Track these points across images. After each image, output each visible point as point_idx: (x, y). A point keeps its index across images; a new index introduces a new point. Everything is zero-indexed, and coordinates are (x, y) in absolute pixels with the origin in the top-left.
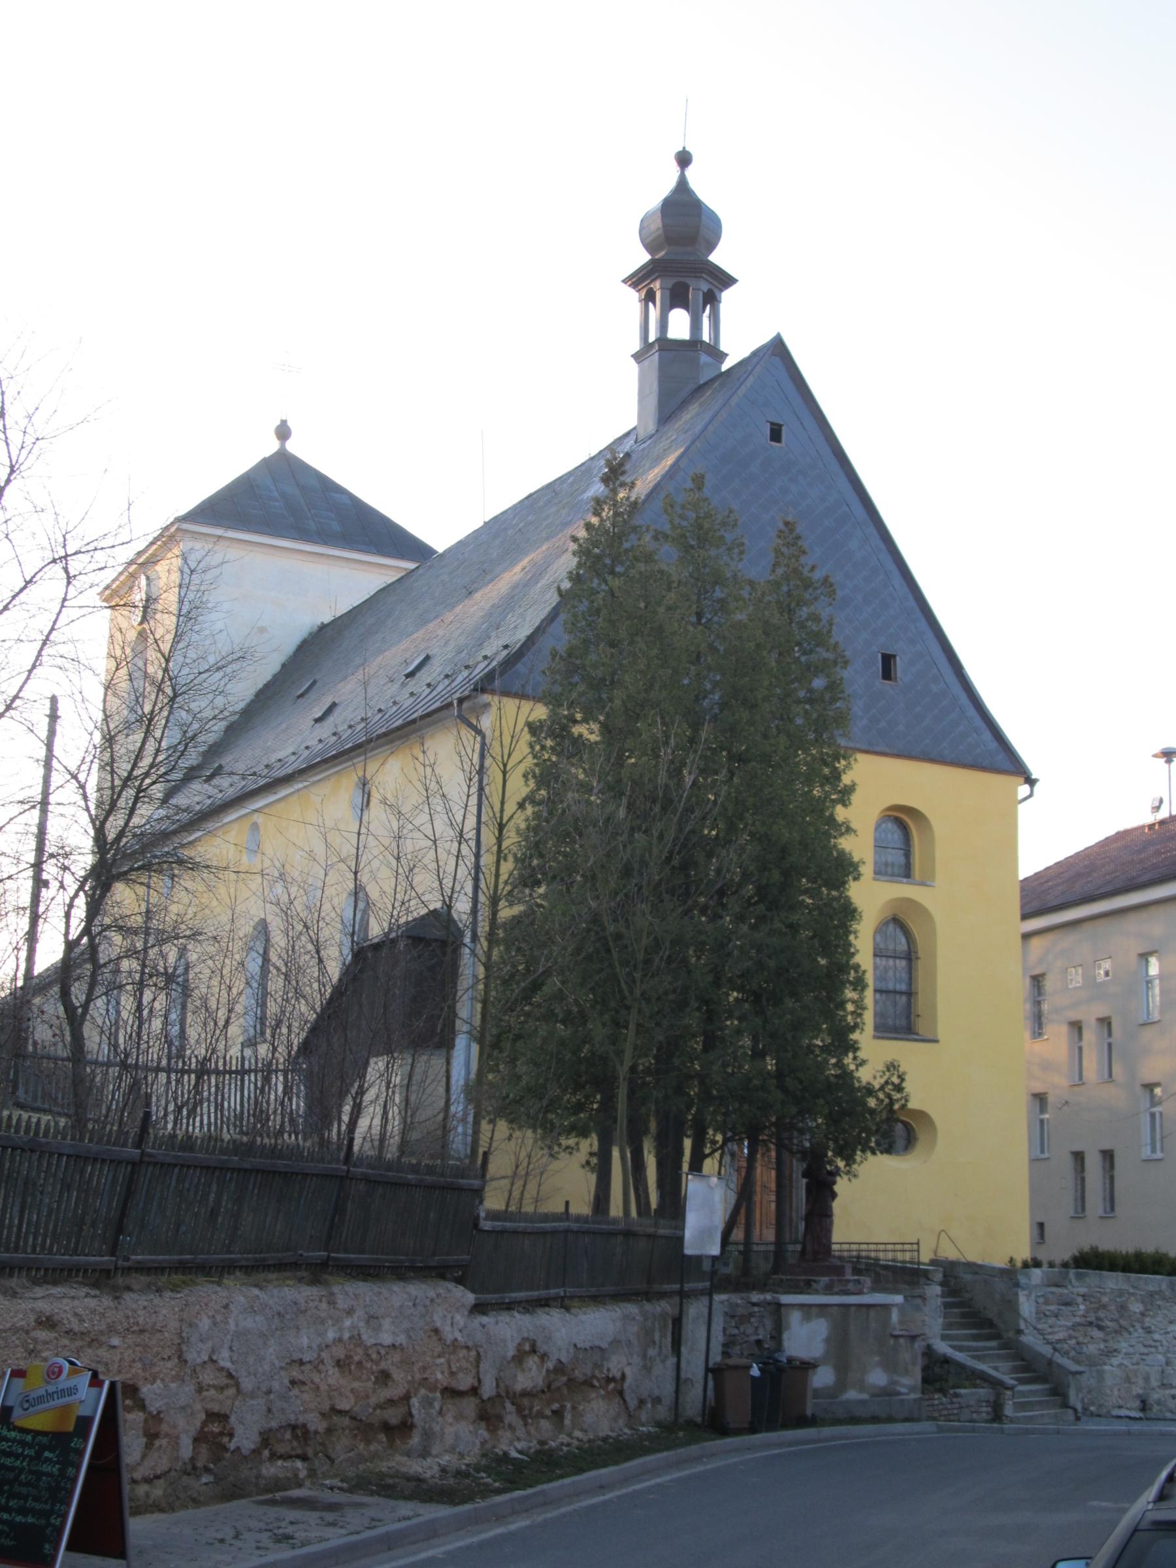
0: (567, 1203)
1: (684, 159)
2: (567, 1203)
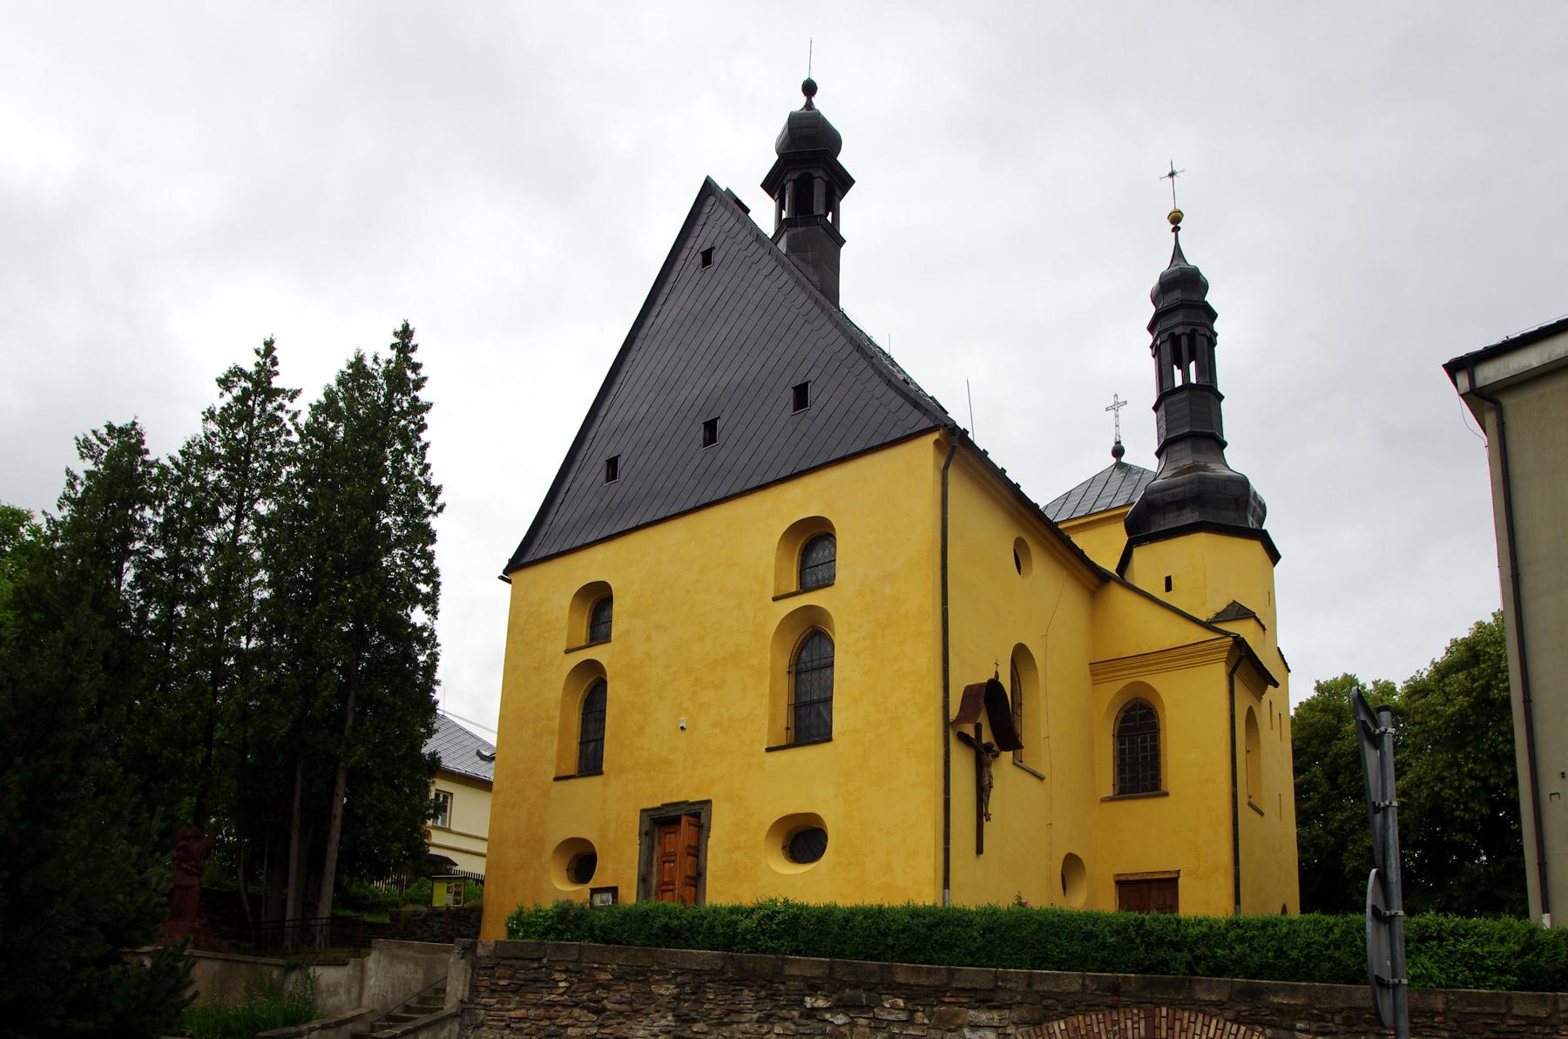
0: (1183, 317)
1: (809, 88)
2: (1183, 317)
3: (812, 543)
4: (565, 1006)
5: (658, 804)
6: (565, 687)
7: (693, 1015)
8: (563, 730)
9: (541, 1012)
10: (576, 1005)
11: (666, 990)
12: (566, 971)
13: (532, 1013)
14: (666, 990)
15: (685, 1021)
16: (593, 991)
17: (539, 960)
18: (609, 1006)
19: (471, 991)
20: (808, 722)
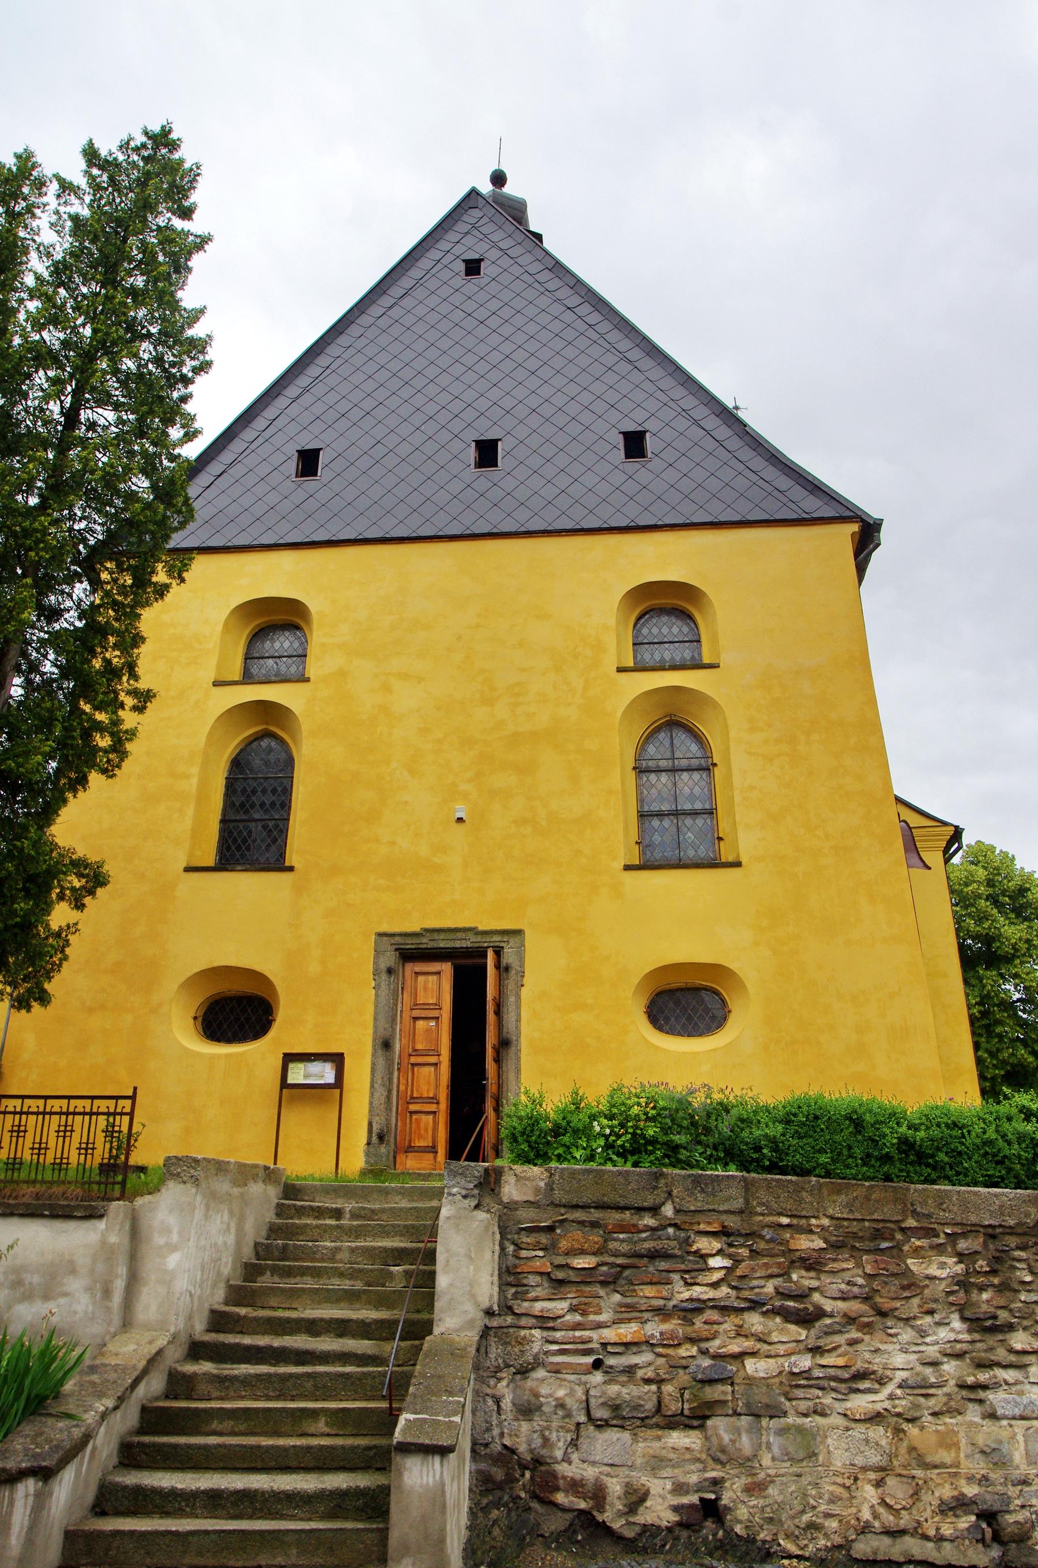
3: (666, 608)
4: (725, 1310)
5: (416, 928)
6: (210, 735)
7: (1003, 1315)
8: (201, 798)
9: (673, 1325)
10: (755, 1305)
11: (941, 1269)
12: (724, 1232)
13: (654, 1328)
14: (941, 1269)
15: (994, 1330)
16: (785, 1274)
17: (654, 1210)
18: (828, 1306)
19: (503, 1285)
20: (678, 835)
